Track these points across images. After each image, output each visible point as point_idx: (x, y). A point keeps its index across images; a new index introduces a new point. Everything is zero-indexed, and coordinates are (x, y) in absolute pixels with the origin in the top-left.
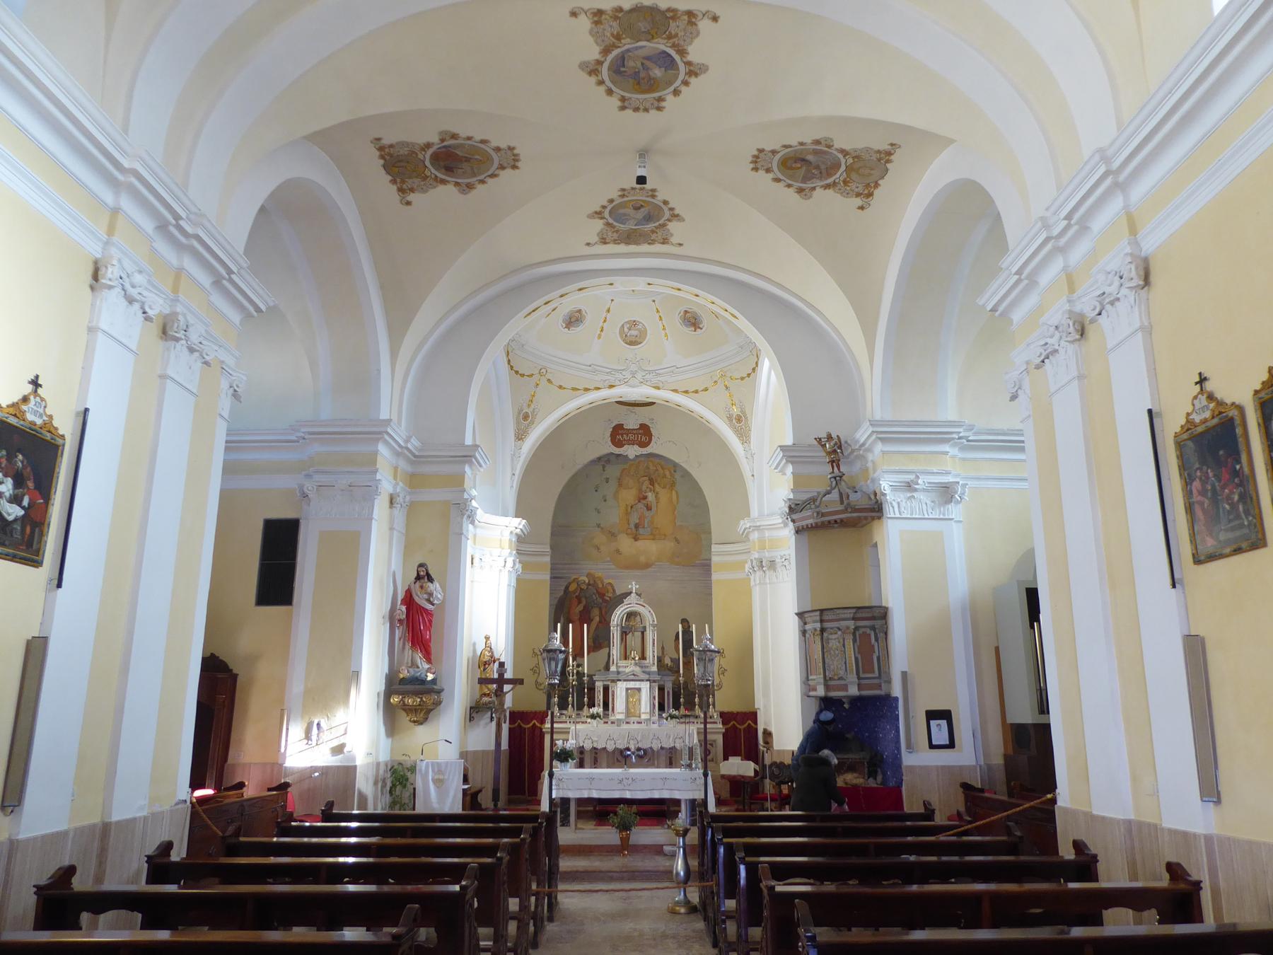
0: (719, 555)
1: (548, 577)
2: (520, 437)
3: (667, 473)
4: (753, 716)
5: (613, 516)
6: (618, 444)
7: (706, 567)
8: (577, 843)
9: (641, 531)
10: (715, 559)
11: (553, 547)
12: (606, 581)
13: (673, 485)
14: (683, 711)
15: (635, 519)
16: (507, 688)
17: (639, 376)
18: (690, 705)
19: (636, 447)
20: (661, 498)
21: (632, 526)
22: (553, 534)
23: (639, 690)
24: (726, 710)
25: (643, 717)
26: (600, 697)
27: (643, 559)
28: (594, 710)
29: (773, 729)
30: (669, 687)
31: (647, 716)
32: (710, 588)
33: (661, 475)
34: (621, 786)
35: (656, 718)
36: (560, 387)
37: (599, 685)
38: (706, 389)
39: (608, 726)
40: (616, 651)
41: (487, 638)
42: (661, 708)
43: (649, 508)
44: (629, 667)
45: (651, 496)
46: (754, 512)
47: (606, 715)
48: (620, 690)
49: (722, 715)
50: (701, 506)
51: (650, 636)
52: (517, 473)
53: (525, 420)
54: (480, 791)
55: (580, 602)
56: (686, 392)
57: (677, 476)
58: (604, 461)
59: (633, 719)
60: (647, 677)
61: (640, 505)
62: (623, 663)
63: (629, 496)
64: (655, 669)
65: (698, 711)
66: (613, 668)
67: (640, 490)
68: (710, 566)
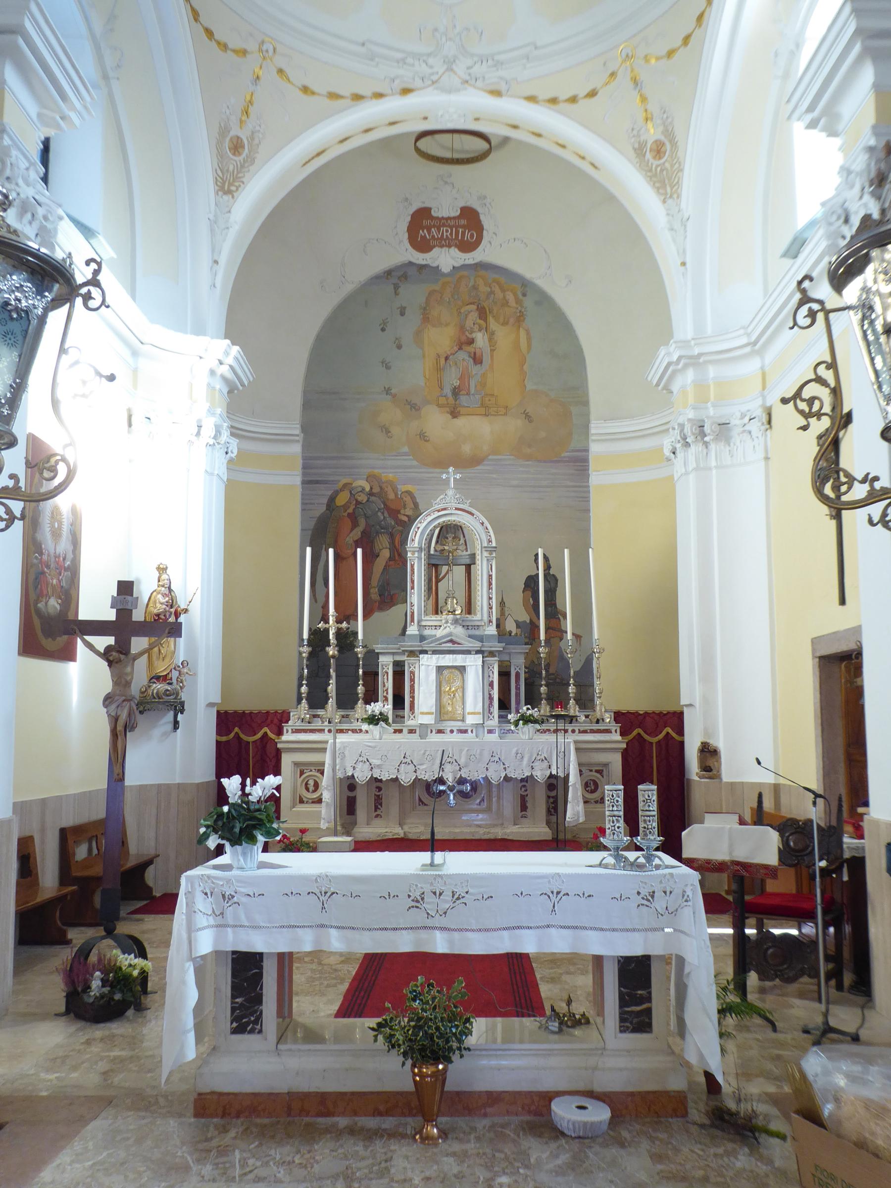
0: (604, 440)
1: (298, 480)
2: (227, 185)
3: (510, 297)
4: (677, 719)
5: (414, 373)
6: (422, 246)
7: (580, 464)
8: (281, 1087)
9: (463, 399)
10: (595, 448)
11: (305, 428)
12: (402, 488)
13: (520, 318)
14: (545, 709)
15: (452, 379)
16: (138, 644)
17: (460, 68)
18: (557, 699)
19: (454, 251)
20: (499, 342)
21: (448, 391)
22: (307, 405)
23: (462, 669)
24: (624, 707)
25: (471, 720)
26: (387, 684)
27: (466, 449)
28: (375, 708)
29: (720, 743)
30: (518, 665)
31: (478, 719)
32: (586, 499)
33: (503, 300)
34: (418, 918)
35: (494, 722)
36: (305, 90)
37: (386, 663)
38: (593, 94)
39: (404, 738)
40: (416, 597)
41: (162, 570)
42: (504, 705)
43: (477, 360)
44: (443, 627)
45: (481, 339)
46: (684, 326)
47: (399, 718)
48: (425, 672)
49: (618, 716)
50: (570, 356)
51: (481, 570)
52: (223, 259)
53: (235, 154)
54: (149, 862)
55: (355, 524)
56: (553, 101)
57: (528, 302)
58: (398, 276)
59: (448, 725)
60: (477, 645)
61: (462, 355)
62: (431, 620)
63: (441, 338)
64: (492, 630)
65: (573, 708)
66: (412, 630)
67: (462, 328)
68: (585, 460)
